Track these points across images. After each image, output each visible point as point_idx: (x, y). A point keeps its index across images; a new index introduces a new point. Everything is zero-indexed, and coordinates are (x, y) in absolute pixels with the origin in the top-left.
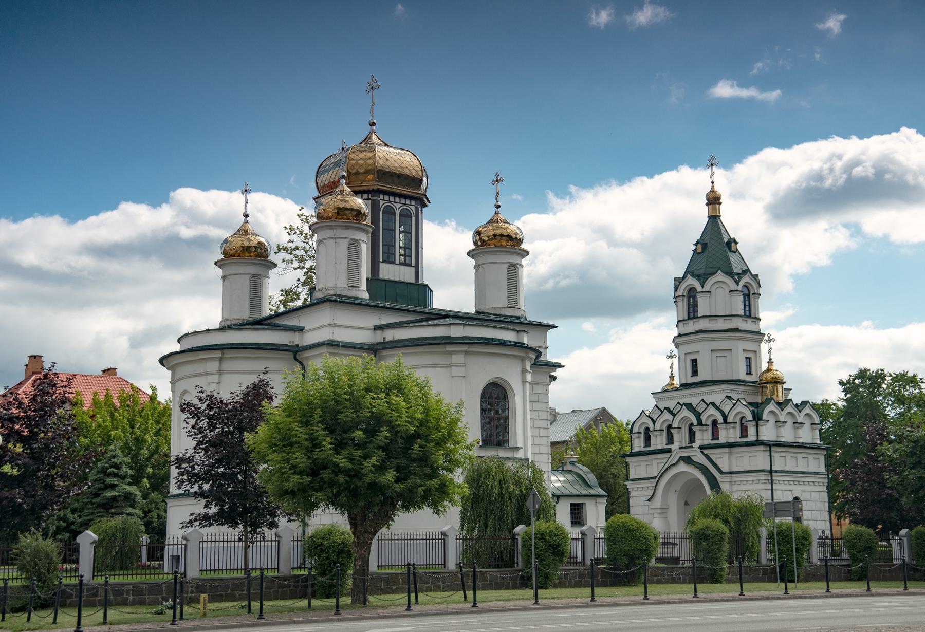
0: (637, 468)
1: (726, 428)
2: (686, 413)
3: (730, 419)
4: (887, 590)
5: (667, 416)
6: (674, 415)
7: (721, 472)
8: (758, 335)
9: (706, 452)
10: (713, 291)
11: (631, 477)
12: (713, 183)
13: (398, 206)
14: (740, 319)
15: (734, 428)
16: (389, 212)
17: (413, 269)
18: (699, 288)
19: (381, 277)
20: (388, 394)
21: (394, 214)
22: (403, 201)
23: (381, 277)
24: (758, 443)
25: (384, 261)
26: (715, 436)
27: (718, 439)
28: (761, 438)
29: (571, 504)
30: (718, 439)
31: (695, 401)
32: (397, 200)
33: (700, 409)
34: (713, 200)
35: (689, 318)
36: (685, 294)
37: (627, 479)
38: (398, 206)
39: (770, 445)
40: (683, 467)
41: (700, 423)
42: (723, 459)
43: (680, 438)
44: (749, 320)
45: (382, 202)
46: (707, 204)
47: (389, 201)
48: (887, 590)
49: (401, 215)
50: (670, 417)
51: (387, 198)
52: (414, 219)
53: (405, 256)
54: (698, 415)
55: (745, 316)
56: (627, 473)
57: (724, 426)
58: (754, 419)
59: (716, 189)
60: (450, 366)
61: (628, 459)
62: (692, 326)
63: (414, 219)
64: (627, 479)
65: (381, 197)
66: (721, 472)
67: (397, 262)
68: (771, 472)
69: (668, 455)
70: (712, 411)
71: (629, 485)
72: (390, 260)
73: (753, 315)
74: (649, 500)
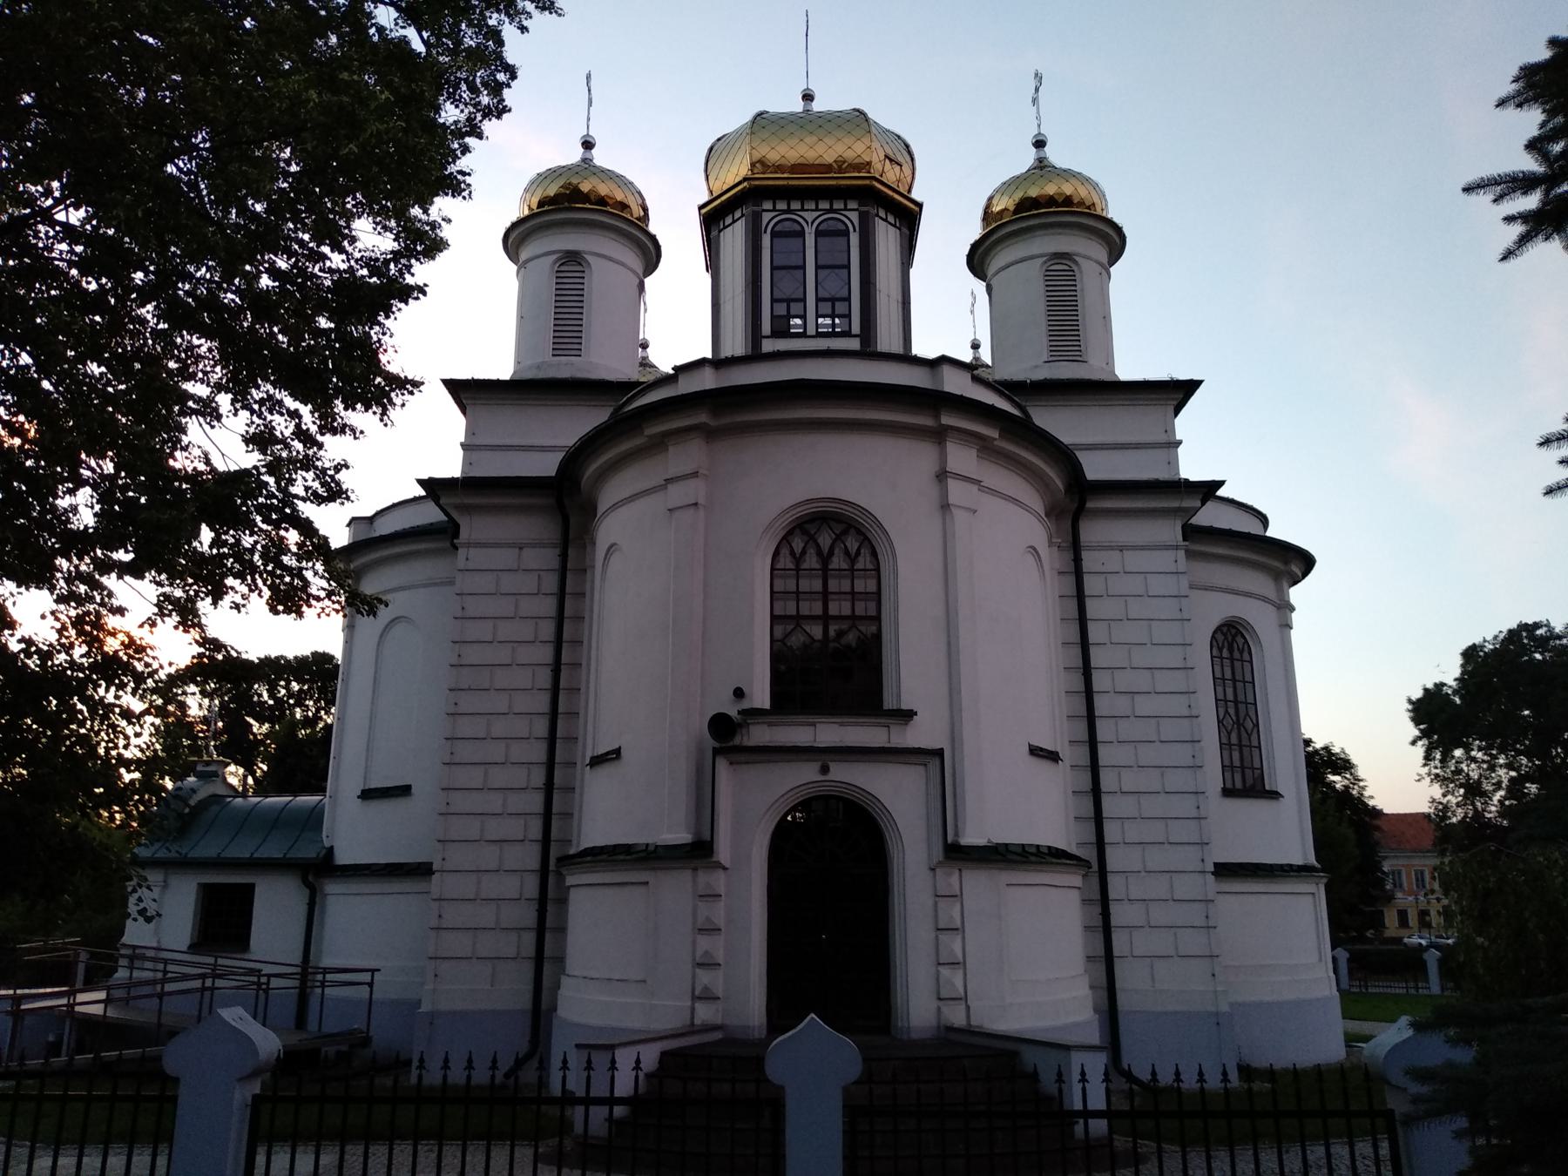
21: (801, 234)
45: (766, 217)
65: (768, 205)
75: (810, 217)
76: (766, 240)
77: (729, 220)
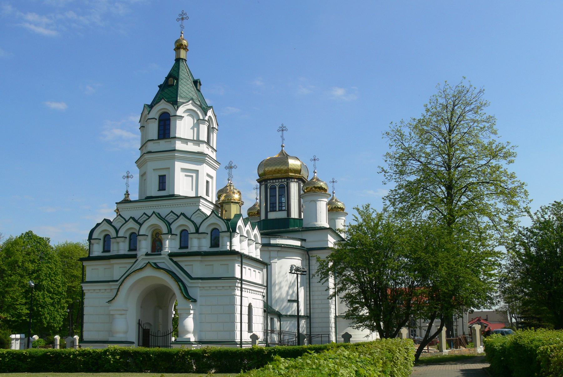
0: (93, 271)
1: (199, 239)
2: (154, 220)
5: (131, 224)
6: (141, 225)
7: (191, 278)
9: (175, 259)
11: (87, 279)
13: (277, 184)
20: (480, 236)
21: (276, 188)
26: (184, 244)
27: (109, 251)
28: (233, 248)
30: (109, 251)
31: (164, 212)
32: (277, 181)
33: (170, 218)
35: (159, 138)
36: (157, 117)
37: (83, 281)
40: (149, 272)
41: (170, 232)
43: (145, 246)
45: (269, 184)
50: (137, 226)
54: (169, 224)
56: (83, 274)
57: (197, 235)
61: (85, 263)
64: (83, 281)
65: (269, 182)
66: (191, 278)
67: (277, 209)
69: (133, 260)
70: (182, 221)
71: (86, 287)
74: (110, 302)
75: (277, 184)
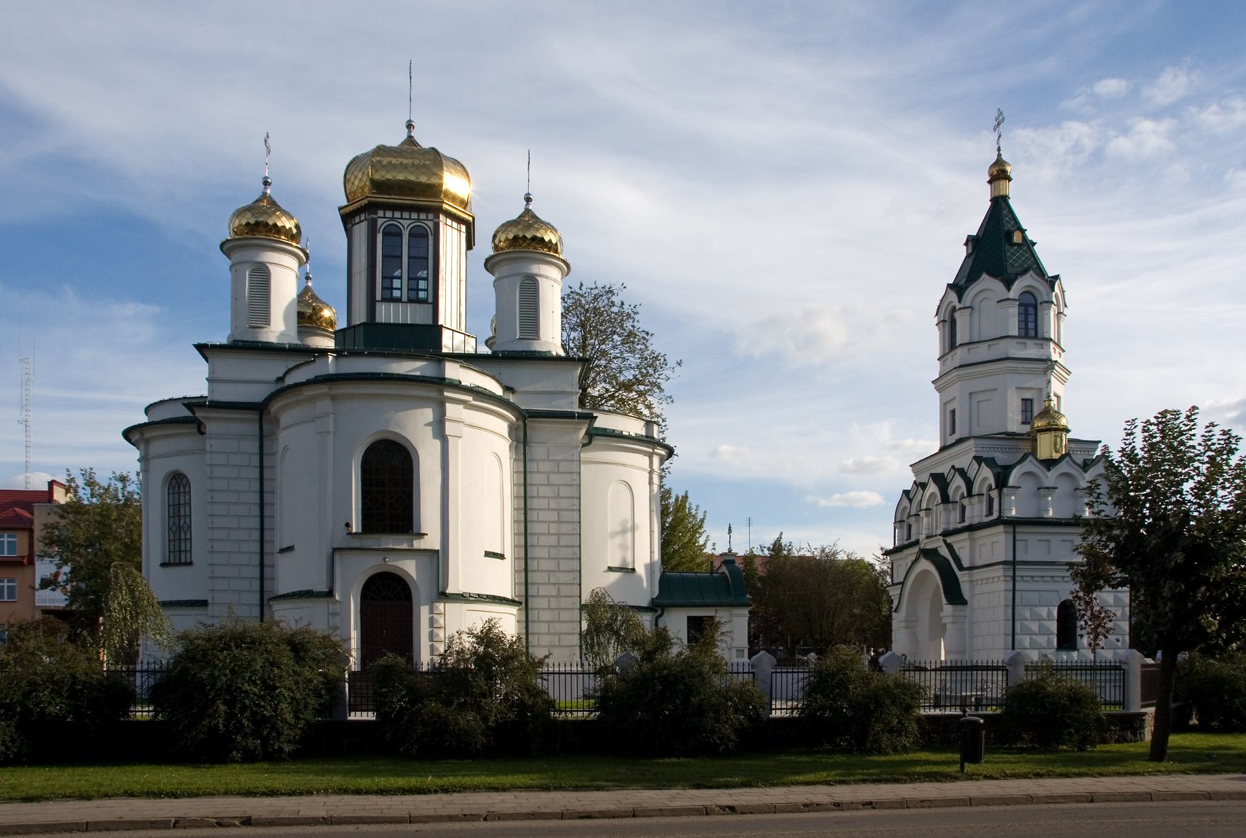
3: (975, 490)
4: (401, 782)
7: (961, 568)
8: (1048, 365)
10: (976, 305)
12: (999, 150)
13: (406, 223)
14: (1013, 342)
15: (980, 502)
16: (393, 234)
17: (430, 307)
18: (958, 306)
19: (378, 320)
21: (400, 235)
22: (414, 216)
23: (378, 320)
24: (1000, 521)
25: (384, 300)
29: (689, 618)
32: (406, 215)
34: (999, 174)
38: (406, 223)
39: (1014, 523)
42: (961, 544)
44: (1030, 343)
45: (380, 221)
46: (990, 182)
47: (419, 220)
48: (401, 782)
49: (410, 235)
51: (389, 214)
52: (431, 238)
53: (418, 290)
55: (1026, 336)
58: (997, 487)
59: (1004, 157)
60: (203, 451)
62: (960, 356)
63: (431, 238)
65: (381, 213)
68: (1013, 564)
72: (389, 299)
73: (1039, 335)
76: (380, 237)
77: (357, 220)
